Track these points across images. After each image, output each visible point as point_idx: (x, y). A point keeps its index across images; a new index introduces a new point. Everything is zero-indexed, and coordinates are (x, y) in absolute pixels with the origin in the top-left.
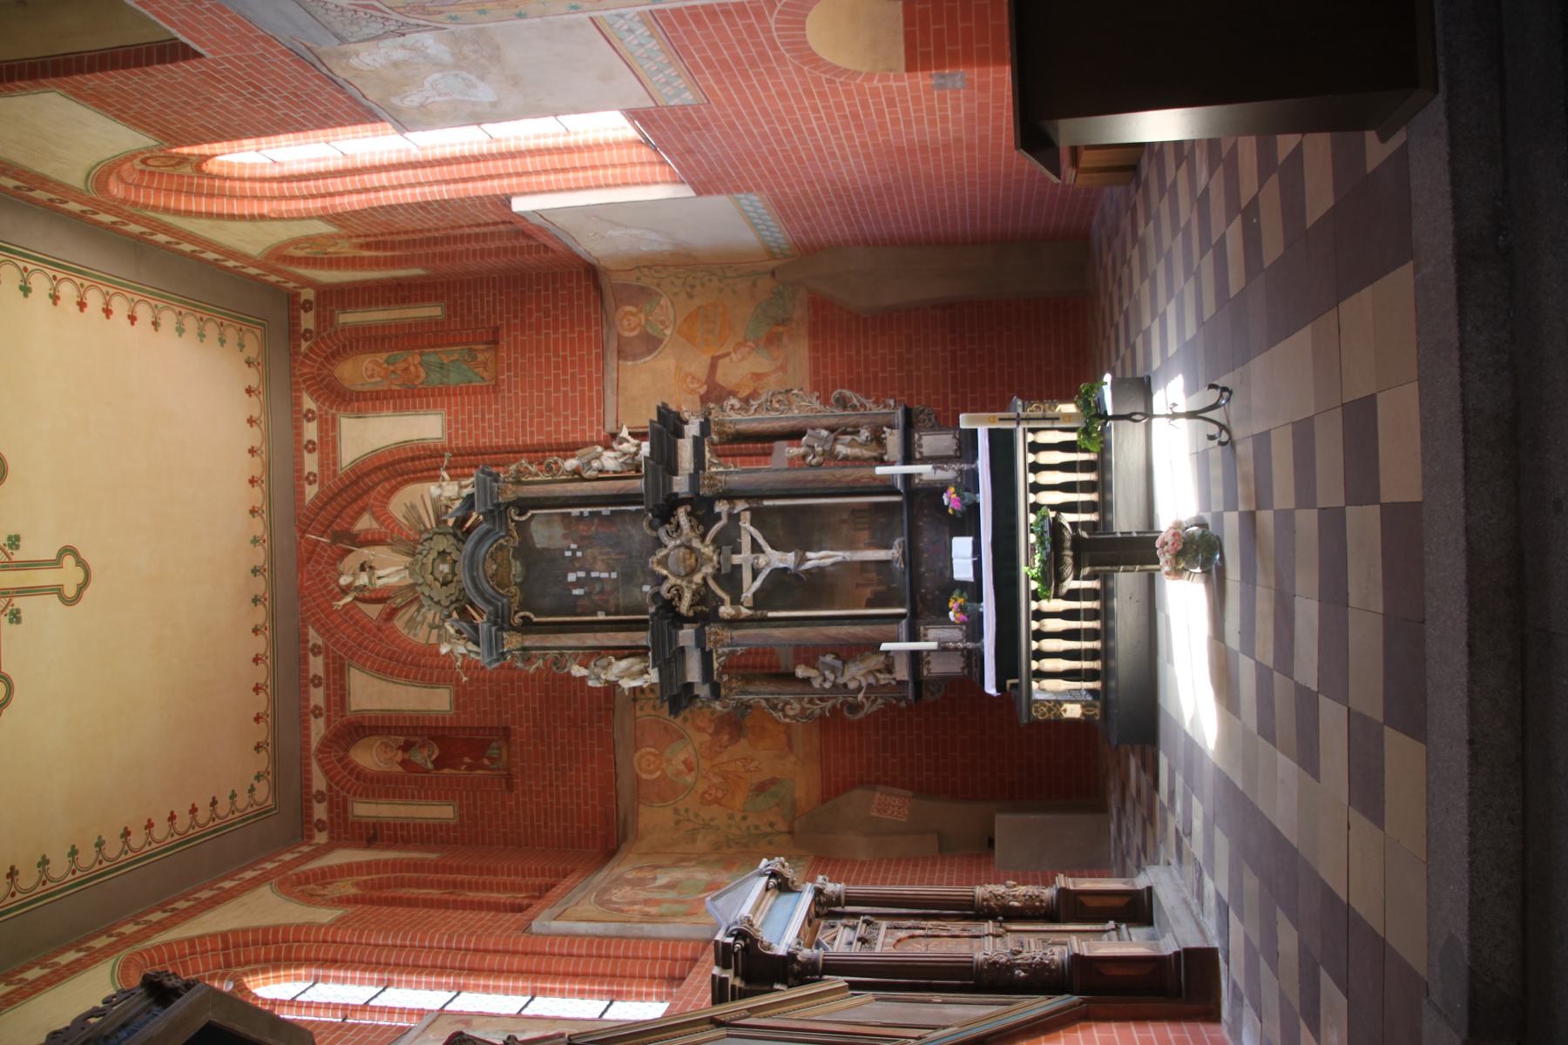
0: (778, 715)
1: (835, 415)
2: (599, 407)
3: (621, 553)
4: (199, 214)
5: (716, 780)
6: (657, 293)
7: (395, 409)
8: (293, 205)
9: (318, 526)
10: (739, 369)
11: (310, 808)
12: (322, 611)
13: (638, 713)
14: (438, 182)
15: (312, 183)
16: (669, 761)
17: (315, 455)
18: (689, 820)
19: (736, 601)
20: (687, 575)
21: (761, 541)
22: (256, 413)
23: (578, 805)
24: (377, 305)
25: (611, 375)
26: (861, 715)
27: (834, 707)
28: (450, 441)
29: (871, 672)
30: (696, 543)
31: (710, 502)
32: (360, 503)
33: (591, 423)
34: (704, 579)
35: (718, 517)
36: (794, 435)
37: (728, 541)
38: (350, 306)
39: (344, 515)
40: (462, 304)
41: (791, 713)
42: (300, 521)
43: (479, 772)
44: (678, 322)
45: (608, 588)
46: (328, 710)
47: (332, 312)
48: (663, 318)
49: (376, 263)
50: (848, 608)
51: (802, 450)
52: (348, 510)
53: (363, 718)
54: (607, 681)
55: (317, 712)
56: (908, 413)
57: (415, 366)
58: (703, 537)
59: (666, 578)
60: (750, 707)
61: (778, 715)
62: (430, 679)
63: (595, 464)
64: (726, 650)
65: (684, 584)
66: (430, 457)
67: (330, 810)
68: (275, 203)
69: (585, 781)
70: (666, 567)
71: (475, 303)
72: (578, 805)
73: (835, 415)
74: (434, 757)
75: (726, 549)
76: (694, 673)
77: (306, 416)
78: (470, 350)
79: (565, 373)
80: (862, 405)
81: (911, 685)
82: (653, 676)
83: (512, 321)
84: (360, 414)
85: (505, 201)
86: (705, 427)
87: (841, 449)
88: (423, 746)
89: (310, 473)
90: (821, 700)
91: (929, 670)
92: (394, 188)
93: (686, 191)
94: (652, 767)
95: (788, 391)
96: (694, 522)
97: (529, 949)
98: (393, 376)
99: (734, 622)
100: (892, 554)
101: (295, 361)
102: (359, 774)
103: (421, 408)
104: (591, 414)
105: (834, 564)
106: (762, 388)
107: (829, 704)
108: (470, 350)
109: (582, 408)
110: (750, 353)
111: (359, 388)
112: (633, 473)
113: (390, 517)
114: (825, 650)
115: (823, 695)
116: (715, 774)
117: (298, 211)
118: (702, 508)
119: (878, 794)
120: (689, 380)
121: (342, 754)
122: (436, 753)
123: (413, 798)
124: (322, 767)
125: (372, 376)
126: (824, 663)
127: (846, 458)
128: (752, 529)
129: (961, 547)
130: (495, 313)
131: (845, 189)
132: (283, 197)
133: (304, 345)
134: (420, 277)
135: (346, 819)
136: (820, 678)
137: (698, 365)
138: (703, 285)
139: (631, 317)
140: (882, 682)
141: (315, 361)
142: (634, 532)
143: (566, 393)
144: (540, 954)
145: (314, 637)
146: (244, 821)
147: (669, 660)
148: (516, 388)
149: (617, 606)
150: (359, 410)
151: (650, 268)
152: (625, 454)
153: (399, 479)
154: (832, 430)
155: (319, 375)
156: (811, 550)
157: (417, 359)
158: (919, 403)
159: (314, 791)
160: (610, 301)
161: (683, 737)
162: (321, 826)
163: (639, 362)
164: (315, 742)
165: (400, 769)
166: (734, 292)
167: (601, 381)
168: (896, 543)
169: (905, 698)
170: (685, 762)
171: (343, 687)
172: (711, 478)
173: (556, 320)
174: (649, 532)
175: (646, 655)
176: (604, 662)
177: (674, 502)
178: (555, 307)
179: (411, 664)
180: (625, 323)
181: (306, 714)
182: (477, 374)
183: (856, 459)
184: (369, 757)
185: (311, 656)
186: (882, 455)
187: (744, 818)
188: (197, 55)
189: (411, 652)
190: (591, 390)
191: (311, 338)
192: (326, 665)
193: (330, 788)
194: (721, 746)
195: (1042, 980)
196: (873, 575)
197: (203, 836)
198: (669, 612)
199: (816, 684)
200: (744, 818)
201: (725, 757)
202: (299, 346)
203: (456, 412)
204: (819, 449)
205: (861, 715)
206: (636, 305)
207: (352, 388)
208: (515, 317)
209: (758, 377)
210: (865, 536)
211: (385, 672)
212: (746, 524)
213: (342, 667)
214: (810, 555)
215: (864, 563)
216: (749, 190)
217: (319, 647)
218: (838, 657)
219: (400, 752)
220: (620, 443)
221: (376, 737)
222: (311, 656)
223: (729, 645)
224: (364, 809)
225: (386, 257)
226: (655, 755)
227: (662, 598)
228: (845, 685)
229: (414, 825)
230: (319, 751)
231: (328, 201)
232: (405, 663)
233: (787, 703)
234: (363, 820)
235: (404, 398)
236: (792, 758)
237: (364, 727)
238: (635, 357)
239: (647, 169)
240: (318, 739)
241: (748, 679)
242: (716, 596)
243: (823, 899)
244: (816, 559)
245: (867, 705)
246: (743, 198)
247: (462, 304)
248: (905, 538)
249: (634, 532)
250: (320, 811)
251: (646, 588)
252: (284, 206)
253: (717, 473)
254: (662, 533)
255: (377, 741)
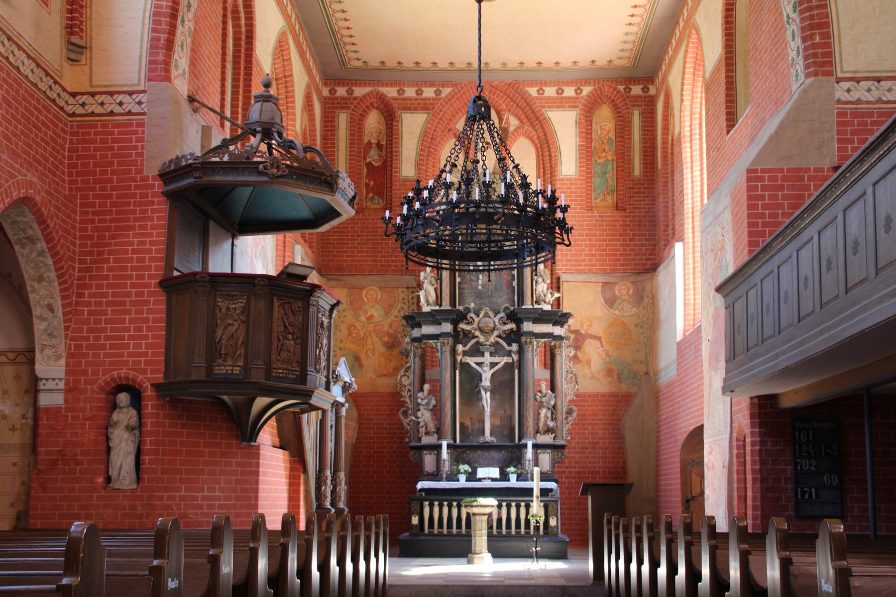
0: (402, 372)
1: (563, 408)
2: (575, 270)
3: (492, 292)
4: (685, 62)
5: (362, 333)
6: (639, 306)
7: (580, 146)
8: (688, 119)
9: (512, 94)
10: (594, 352)
11: (343, 85)
12: (461, 96)
13: (400, 290)
14: (693, 203)
15: (698, 131)
16: (373, 307)
17: (555, 95)
18: (339, 317)
19: (465, 353)
20: (479, 328)
21: (496, 368)
22: (581, 64)
23: (347, 252)
24: (643, 135)
25: (593, 278)
26: (401, 417)
27: (406, 403)
28: (559, 180)
29: (426, 424)
30: (496, 333)
31: (518, 341)
32: (525, 120)
33: (566, 265)
34: (477, 337)
35: (509, 345)
36: (553, 388)
37: (497, 350)
38: (644, 117)
39: (519, 109)
40: (640, 188)
41: (403, 380)
42: (515, 84)
43: (365, 191)
44: (622, 319)
45: (473, 284)
46: (402, 99)
47: (640, 106)
48: (625, 309)
49: (665, 142)
50: (460, 413)
51: (544, 391)
52: (521, 112)
53: (398, 122)
54: (423, 282)
55: (401, 92)
56: (562, 447)
57: (606, 156)
58: (499, 336)
59: (478, 316)
60: (407, 358)
61: (402, 372)
62: (420, 164)
63: (540, 280)
64: (439, 347)
65: (475, 326)
66: (551, 166)
67: (342, 98)
68: (689, 108)
69: (361, 256)
70: (484, 316)
71: (640, 197)
72: (347, 252)
73: (563, 408)
74: (373, 163)
75: (492, 349)
76: (427, 330)
77: (579, 88)
78: (614, 191)
79: (596, 250)
80: (568, 423)
81: (419, 444)
82: (426, 309)
83: (628, 219)
84: (578, 123)
85: (681, 239)
86: (560, 338)
87: (543, 412)
88: (380, 156)
89: (544, 91)
90: (410, 396)
91: (426, 454)
92: (692, 178)
93: (679, 336)
94: (369, 297)
95: (577, 383)
96: (507, 332)
97: (287, 244)
98: (600, 142)
99: (454, 352)
100: (488, 437)
101: (612, 82)
102: (363, 116)
103: (580, 162)
104: (571, 265)
105: (483, 406)
106: (582, 366)
107: (407, 400)
108: (614, 191)
109: (575, 260)
110: (602, 359)
111: (594, 121)
112: (535, 299)
113: (516, 138)
114: (439, 401)
115: (414, 398)
116: (365, 333)
117: (684, 122)
118: (514, 336)
119: (354, 424)
120: (589, 323)
121: (376, 105)
122: (376, 164)
123: (350, 151)
124: (368, 94)
125: (601, 129)
126: (431, 399)
127: (539, 414)
128: (503, 363)
129: (495, 472)
130: (634, 208)
131: (677, 419)
132: (692, 114)
133: (621, 88)
134: (657, 167)
135: (337, 108)
136: (422, 397)
137: (597, 329)
138: (642, 333)
139: (626, 291)
140: (420, 430)
141: (612, 94)
142: (503, 299)
143: (584, 250)
144: (284, 250)
145: (446, 91)
146: (341, 56)
147: (435, 318)
148: (589, 221)
149: (464, 289)
150: (580, 123)
151: (653, 304)
152: (545, 296)
153: (539, 145)
154: (554, 407)
155: (603, 96)
156: (491, 394)
157: (610, 158)
158: (569, 453)
159: (354, 88)
160: (634, 278)
161: (386, 315)
162: (333, 92)
163: (600, 295)
164: (384, 90)
165: (366, 141)
166: (638, 351)
167: (591, 272)
168: (494, 439)
169: (410, 441)
170: (372, 316)
171: (416, 109)
172: (531, 343)
173: (628, 245)
174: (503, 307)
175: (437, 304)
176: (434, 282)
177: (519, 322)
178: (635, 245)
179: (429, 151)
180: (623, 287)
181: (399, 85)
182: (599, 195)
183: (538, 419)
184: (373, 122)
185: (435, 89)
186: (540, 433)
187: (340, 349)
188: (728, 132)
189: (436, 150)
190: (586, 265)
191: (626, 92)
192: (429, 99)
193: (355, 99)
194: (381, 337)
195: (320, 496)
196: (477, 426)
197: (335, 39)
198: (462, 317)
199: (420, 395)
200: (340, 349)
201: (375, 339)
202: (621, 85)
203: (577, 184)
204: (544, 400)
205: (401, 417)
206: (633, 294)
207: (595, 115)
208: (631, 221)
209: (589, 363)
210: (498, 422)
211: (424, 136)
212: (506, 360)
213: (428, 109)
214: (488, 393)
215: (483, 422)
216: (678, 371)
217: (440, 95)
218: (434, 406)
219: (376, 141)
220: (551, 293)
221: (385, 127)
222: (435, 89)
223: (441, 350)
224: (343, 119)
225: (668, 148)
226: (376, 298)
227: (467, 314)
228: (419, 410)
229: (334, 151)
230: (378, 92)
231: (688, 139)
232: (429, 147)
233: (409, 377)
234: (336, 119)
235: (587, 151)
236: (374, 377)
237: (392, 120)
238: (603, 292)
239: (692, 317)
240: (385, 92)
241: (423, 358)
242: (468, 343)
243: (339, 406)
244: (486, 397)
245: (407, 421)
246: (675, 366)
247: (640, 188)
248: (496, 443)
249: (503, 299)
250: (341, 91)
251: (473, 305)
252: (687, 113)
253: (533, 345)
254: (502, 314)
255: (383, 128)
